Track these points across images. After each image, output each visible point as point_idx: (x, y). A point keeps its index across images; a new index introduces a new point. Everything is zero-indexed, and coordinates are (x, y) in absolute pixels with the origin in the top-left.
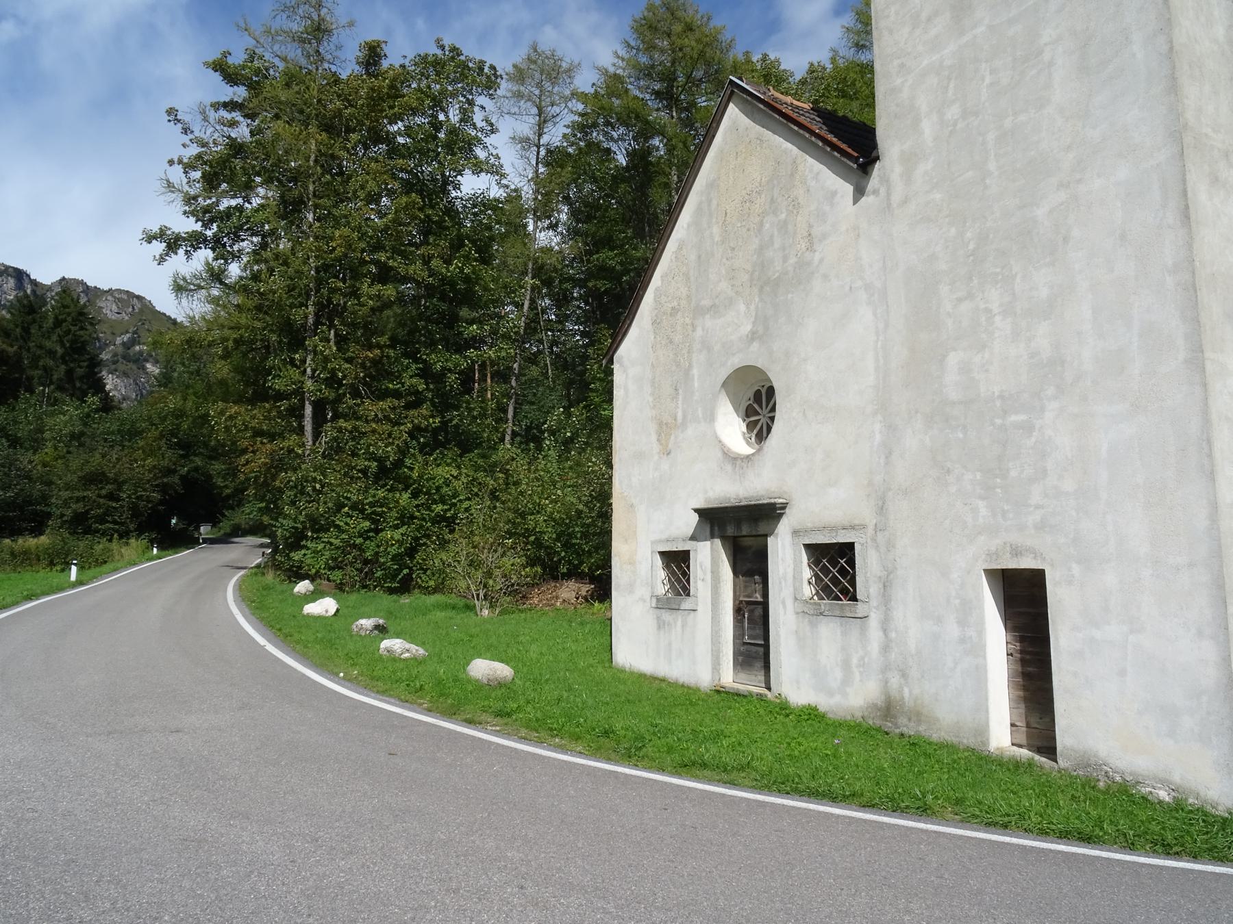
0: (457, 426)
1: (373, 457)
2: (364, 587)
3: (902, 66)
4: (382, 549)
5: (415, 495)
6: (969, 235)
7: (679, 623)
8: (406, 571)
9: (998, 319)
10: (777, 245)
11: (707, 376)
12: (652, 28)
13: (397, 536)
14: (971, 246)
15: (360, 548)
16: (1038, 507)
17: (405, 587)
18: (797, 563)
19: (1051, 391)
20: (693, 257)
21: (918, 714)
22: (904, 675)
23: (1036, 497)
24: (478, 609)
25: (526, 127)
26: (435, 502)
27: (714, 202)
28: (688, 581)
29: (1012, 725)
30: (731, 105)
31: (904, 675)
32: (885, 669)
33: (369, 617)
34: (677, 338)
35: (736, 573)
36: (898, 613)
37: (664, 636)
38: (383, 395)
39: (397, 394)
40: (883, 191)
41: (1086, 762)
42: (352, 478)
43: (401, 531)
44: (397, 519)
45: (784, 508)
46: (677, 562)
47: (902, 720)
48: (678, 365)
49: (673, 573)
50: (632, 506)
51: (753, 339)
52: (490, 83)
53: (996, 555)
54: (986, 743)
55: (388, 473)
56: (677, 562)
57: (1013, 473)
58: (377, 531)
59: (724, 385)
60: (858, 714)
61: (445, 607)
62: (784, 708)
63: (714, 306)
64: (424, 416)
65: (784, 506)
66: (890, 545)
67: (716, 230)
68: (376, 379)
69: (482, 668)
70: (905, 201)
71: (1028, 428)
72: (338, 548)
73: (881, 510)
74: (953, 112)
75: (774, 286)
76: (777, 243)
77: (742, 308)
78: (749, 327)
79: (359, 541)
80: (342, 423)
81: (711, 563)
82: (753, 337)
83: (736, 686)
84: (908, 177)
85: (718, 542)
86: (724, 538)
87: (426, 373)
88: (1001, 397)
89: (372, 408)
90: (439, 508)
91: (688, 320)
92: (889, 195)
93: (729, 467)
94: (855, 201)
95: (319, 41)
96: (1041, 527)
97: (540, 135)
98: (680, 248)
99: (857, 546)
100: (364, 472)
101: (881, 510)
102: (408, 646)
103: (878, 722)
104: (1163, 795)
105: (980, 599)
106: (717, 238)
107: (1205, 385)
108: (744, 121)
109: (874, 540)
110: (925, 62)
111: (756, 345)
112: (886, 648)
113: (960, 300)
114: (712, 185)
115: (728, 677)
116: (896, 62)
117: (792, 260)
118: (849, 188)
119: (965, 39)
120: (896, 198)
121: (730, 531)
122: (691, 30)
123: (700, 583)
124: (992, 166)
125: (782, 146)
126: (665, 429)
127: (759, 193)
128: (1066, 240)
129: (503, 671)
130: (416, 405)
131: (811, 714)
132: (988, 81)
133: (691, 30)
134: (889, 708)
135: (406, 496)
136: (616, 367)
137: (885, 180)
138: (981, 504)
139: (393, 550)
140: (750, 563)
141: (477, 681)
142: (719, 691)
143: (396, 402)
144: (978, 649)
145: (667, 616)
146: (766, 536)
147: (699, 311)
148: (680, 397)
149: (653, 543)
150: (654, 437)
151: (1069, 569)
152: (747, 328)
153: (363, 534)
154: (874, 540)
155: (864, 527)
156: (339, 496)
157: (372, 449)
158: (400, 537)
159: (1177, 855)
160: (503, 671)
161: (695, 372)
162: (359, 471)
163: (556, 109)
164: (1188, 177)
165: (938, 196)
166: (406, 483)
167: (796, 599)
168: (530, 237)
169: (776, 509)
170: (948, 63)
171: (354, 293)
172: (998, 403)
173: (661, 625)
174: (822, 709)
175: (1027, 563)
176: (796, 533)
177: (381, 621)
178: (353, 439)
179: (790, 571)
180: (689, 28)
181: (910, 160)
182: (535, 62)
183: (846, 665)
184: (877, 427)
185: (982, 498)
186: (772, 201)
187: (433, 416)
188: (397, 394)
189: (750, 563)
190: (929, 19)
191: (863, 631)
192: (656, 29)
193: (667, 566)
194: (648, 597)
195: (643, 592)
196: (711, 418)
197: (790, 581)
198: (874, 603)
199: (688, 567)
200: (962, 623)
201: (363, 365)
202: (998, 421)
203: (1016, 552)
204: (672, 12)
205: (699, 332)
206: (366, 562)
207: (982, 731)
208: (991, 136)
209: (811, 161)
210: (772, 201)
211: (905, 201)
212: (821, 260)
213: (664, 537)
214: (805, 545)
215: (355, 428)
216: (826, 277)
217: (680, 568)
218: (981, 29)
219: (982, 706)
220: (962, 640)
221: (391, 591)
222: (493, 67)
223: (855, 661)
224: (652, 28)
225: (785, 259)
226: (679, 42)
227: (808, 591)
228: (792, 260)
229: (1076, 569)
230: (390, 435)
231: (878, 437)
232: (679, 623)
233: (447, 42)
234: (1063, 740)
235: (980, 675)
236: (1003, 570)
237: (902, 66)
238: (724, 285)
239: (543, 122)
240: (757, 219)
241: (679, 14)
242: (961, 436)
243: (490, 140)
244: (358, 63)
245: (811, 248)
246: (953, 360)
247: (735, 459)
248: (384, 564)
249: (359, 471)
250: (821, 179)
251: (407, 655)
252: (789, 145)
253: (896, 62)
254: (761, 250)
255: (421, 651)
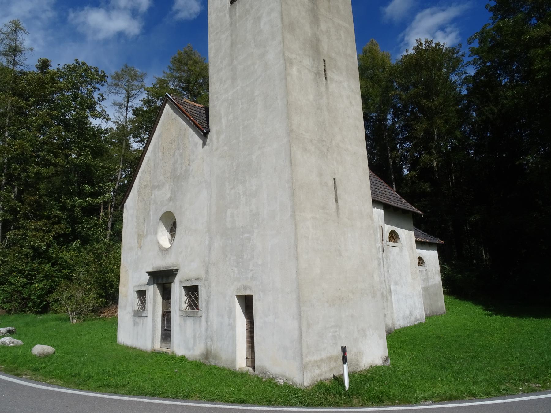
0: (80, 232)
1: (32, 247)
2: (22, 311)
3: (217, 97)
4: (33, 292)
5: (53, 265)
6: (234, 164)
7: (141, 323)
8: (45, 303)
9: (242, 197)
10: (179, 162)
11: (155, 215)
12: (180, 61)
13: (41, 286)
14: (235, 168)
15: (20, 292)
16: (252, 270)
17: (45, 310)
18: (181, 294)
19: (256, 225)
20: (152, 165)
21: (216, 356)
22: (212, 340)
23: (251, 267)
24: (71, 319)
25: (120, 98)
26: (64, 268)
27: (160, 143)
28: (198, 302)
29: (247, 358)
30: (167, 104)
31: (212, 340)
32: (206, 338)
33: (5, 327)
34: (146, 198)
35: (163, 298)
36: (211, 315)
37: (135, 329)
38: (41, 218)
39: (49, 218)
40: (210, 144)
41: (264, 371)
42: (20, 258)
43: (43, 283)
44: (43, 277)
45: (177, 271)
46: (142, 294)
47: (211, 359)
48: (146, 210)
49: (190, 297)
50: (127, 271)
51: (170, 200)
52: (102, 79)
53: (239, 290)
54: (234, 366)
55: (38, 254)
56: (142, 294)
57: (245, 257)
58: (31, 284)
59: (161, 219)
60: (198, 358)
61: (56, 319)
62: (173, 357)
63: (158, 186)
64: (60, 228)
65: (177, 271)
66: (209, 286)
67: (160, 154)
68: (38, 211)
69: (38, 349)
70: (217, 149)
71: (249, 239)
72: (9, 293)
73: (207, 272)
74: (231, 117)
75: (178, 178)
76: (179, 160)
77: (167, 187)
78: (169, 195)
79: (21, 288)
80: (17, 231)
81: (154, 294)
82: (170, 199)
83: (161, 349)
84: (218, 139)
85: (156, 285)
86: (158, 285)
87: (63, 208)
88: (242, 227)
89: (32, 224)
90: (65, 271)
91: (150, 191)
92: (212, 146)
93: (160, 254)
94: (203, 147)
95: (15, 55)
96: (253, 278)
97: (128, 102)
98: (148, 160)
99: (199, 287)
100: (26, 255)
101: (207, 272)
102: (13, 340)
103: (204, 361)
104: (282, 382)
105: (234, 307)
106: (161, 158)
107: (296, 225)
108: (171, 111)
109: (204, 284)
110: (224, 97)
111: (171, 202)
112: (207, 330)
113: (231, 189)
114: (159, 136)
115: (158, 345)
116: (215, 96)
117: (184, 169)
118: (201, 142)
119: (234, 90)
120: (214, 147)
121: (160, 281)
122: (197, 63)
123: (149, 304)
124: (241, 139)
125: (182, 122)
126: (140, 237)
127: (174, 141)
128: (260, 168)
129: (48, 349)
130: (59, 223)
131: (183, 359)
132: (240, 107)
133: (197, 63)
134: (207, 355)
135: (48, 266)
136: (124, 209)
137: (211, 140)
138: (236, 269)
139: (38, 293)
140: (166, 294)
141: (35, 355)
142: (155, 353)
143: (47, 222)
144: (232, 327)
145: (137, 319)
146: (171, 283)
147: (153, 187)
148: (146, 224)
149: (134, 287)
150: (136, 241)
151: (259, 294)
152: (169, 195)
153: (23, 286)
154: (204, 284)
155: (201, 279)
156: (11, 267)
157: (32, 243)
158: (42, 286)
159: (273, 405)
160: (48, 349)
161: (151, 213)
162: (24, 255)
163: (133, 92)
164: (292, 149)
165: (226, 148)
166: (49, 259)
167: (180, 310)
168: (128, 145)
169: (173, 272)
170: (230, 98)
171: (25, 170)
172: (241, 229)
173: (135, 324)
174: (186, 357)
175: (248, 293)
176: (181, 282)
177: (11, 329)
178: (23, 239)
179: (178, 297)
180: (196, 62)
181: (218, 133)
182: (126, 72)
183: (194, 337)
184: (207, 238)
185: (236, 267)
186: (178, 145)
187: (66, 228)
188: (49, 218)
189: (166, 294)
190: (225, 81)
191: (200, 321)
192: (181, 62)
193: (187, 294)
194: (131, 311)
195: (129, 309)
196: (156, 233)
197: (178, 302)
198: (204, 310)
199: (198, 294)
200: (229, 317)
201: (29, 204)
202: (241, 236)
203: (245, 288)
204: (189, 56)
205: (153, 196)
206: (24, 299)
207: (234, 361)
208: (241, 127)
209: (191, 130)
210: (178, 145)
211: (217, 149)
212: (192, 170)
213: (137, 284)
214: (184, 287)
215: (24, 234)
216: (193, 176)
217: (193, 294)
218: (239, 88)
219: (234, 352)
220: (229, 325)
221: (37, 313)
222: (103, 72)
223: (197, 335)
224: (180, 61)
225: (181, 168)
226: (191, 68)
227: (184, 306)
228: (184, 169)
229: (261, 294)
230: (43, 237)
231: (207, 242)
232: (141, 323)
233: (81, 61)
234: (257, 363)
235: (233, 338)
236: (245, 295)
237: (217, 97)
238: (162, 177)
239: (129, 97)
240: (173, 151)
241: (192, 56)
242: (230, 242)
243: (103, 103)
244: (37, 67)
245: (189, 165)
246: (229, 212)
247: (163, 250)
248: (33, 300)
249: (24, 255)
250: (193, 137)
251: (12, 345)
252: (184, 123)
253: (215, 96)
254: (175, 163)
255: (20, 342)
